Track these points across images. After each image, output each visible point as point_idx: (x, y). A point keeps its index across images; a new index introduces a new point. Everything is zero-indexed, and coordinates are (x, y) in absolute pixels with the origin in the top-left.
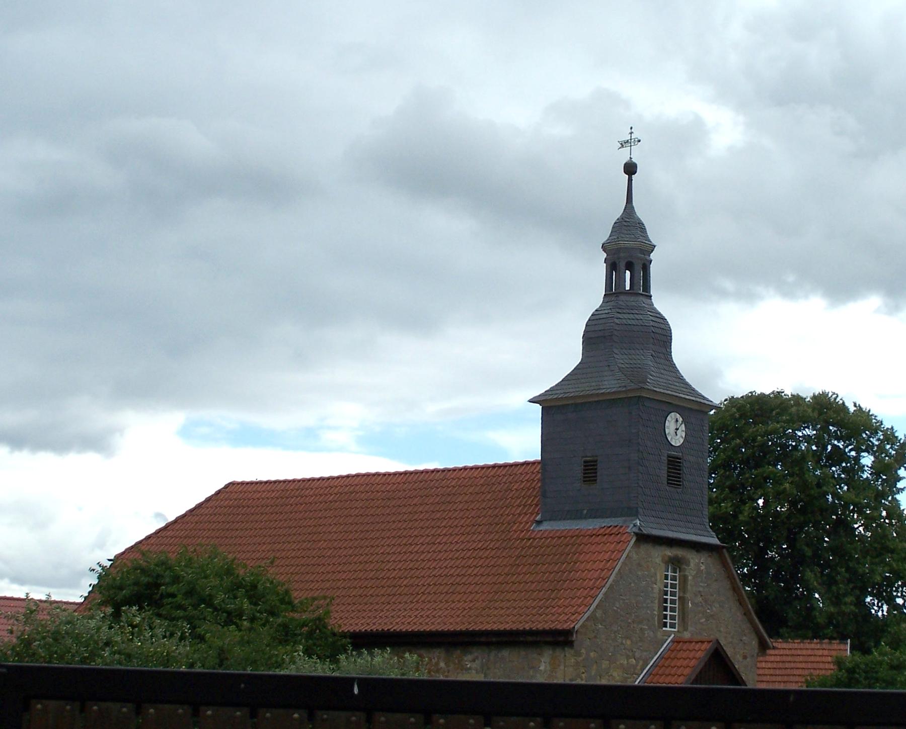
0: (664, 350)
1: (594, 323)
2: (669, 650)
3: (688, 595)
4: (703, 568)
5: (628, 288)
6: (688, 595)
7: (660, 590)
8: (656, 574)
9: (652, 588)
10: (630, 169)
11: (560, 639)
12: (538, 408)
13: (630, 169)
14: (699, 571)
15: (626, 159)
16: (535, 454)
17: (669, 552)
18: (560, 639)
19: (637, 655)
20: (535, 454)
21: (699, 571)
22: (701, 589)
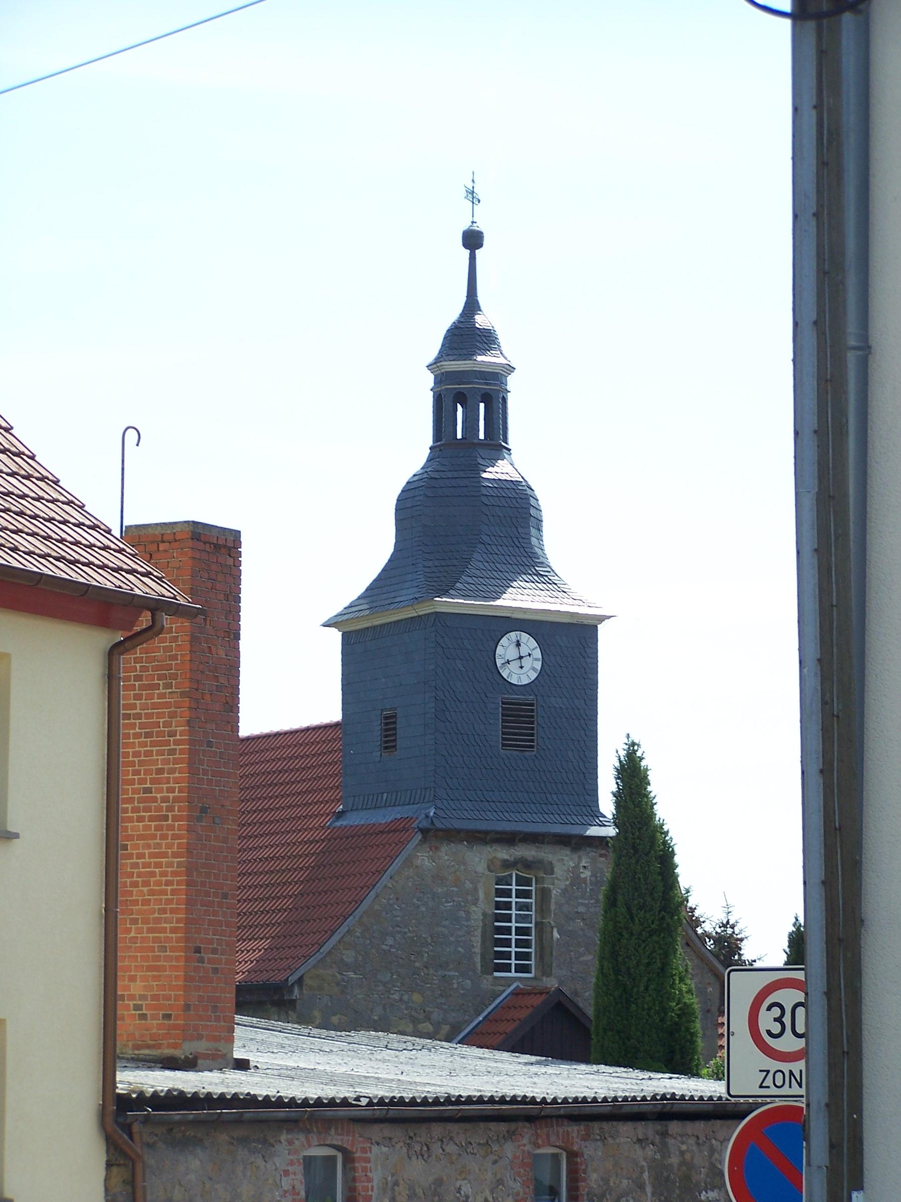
0: (230, 561)
1: (411, 494)
2: (502, 1007)
3: (551, 920)
4: (586, 874)
5: (482, 436)
6: (551, 920)
7: (485, 914)
8: (476, 889)
9: (468, 913)
10: (473, 240)
11: (801, 1071)
12: (336, 636)
13: (473, 240)
14: (576, 881)
15: (466, 225)
16: (334, 714)
17: (503, 853)
18: (801, 1071)
19: (436, 1016)
20: (334, 714)
21: (576, 881)
22: (581, 909)
